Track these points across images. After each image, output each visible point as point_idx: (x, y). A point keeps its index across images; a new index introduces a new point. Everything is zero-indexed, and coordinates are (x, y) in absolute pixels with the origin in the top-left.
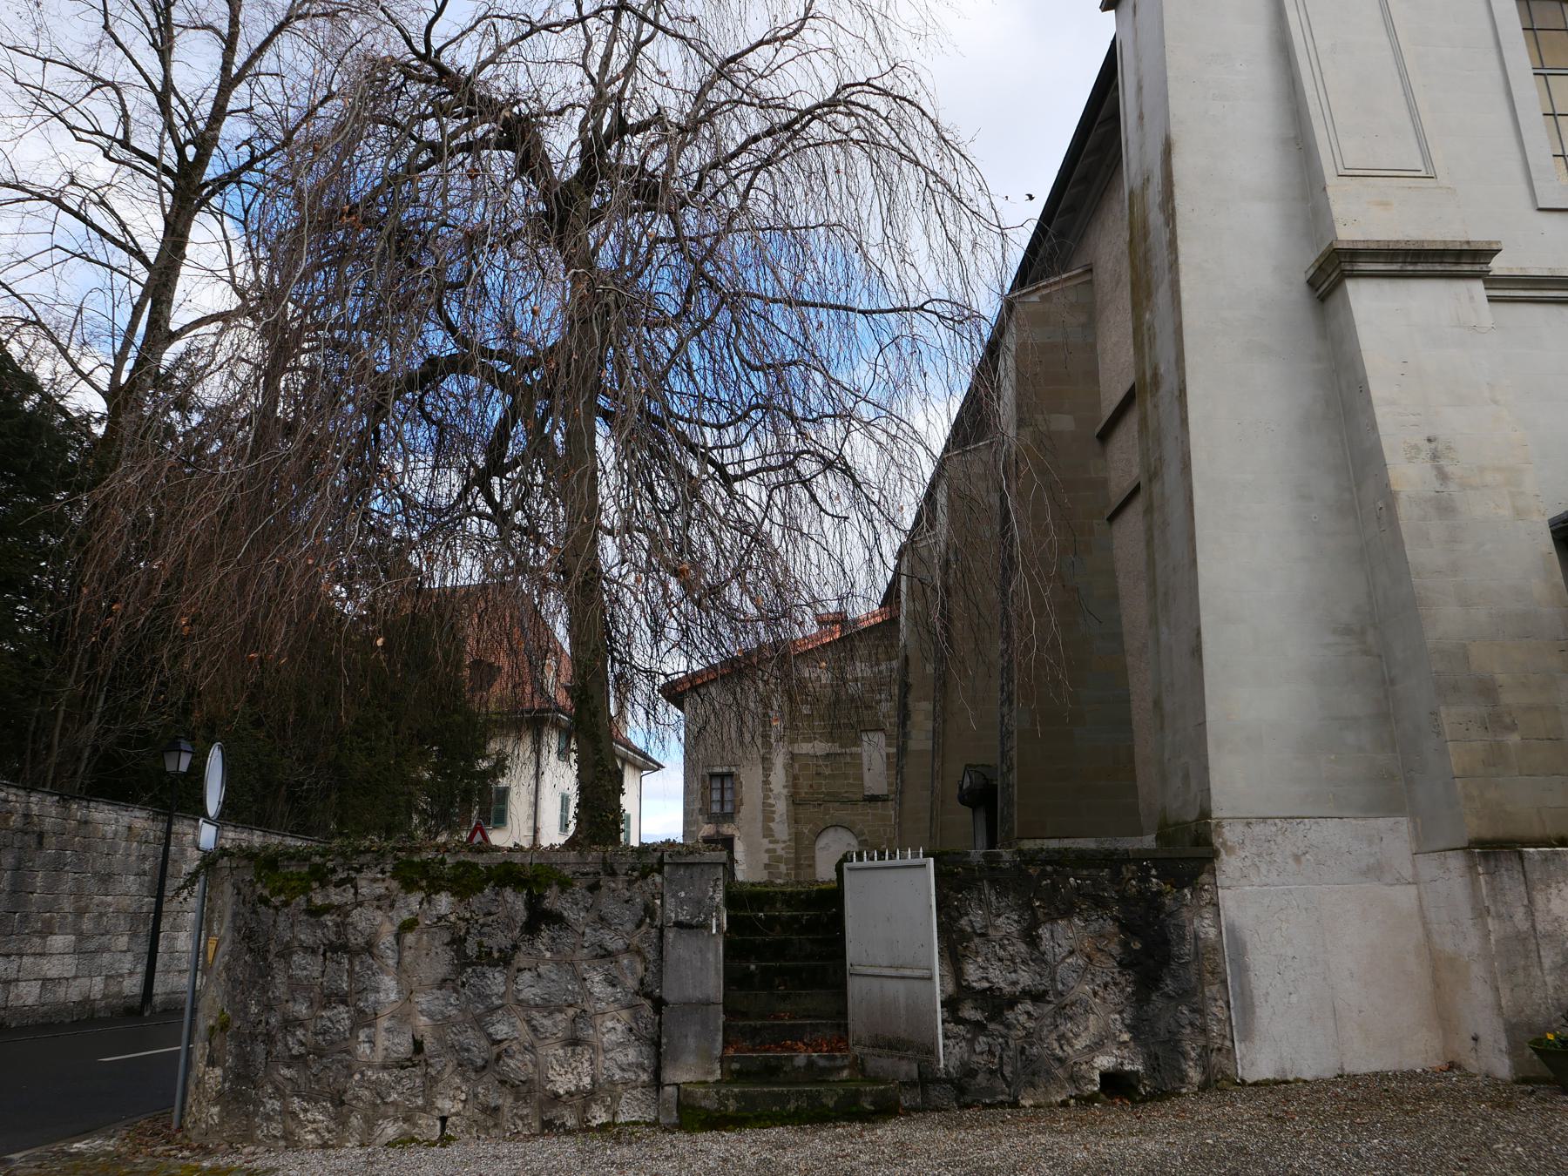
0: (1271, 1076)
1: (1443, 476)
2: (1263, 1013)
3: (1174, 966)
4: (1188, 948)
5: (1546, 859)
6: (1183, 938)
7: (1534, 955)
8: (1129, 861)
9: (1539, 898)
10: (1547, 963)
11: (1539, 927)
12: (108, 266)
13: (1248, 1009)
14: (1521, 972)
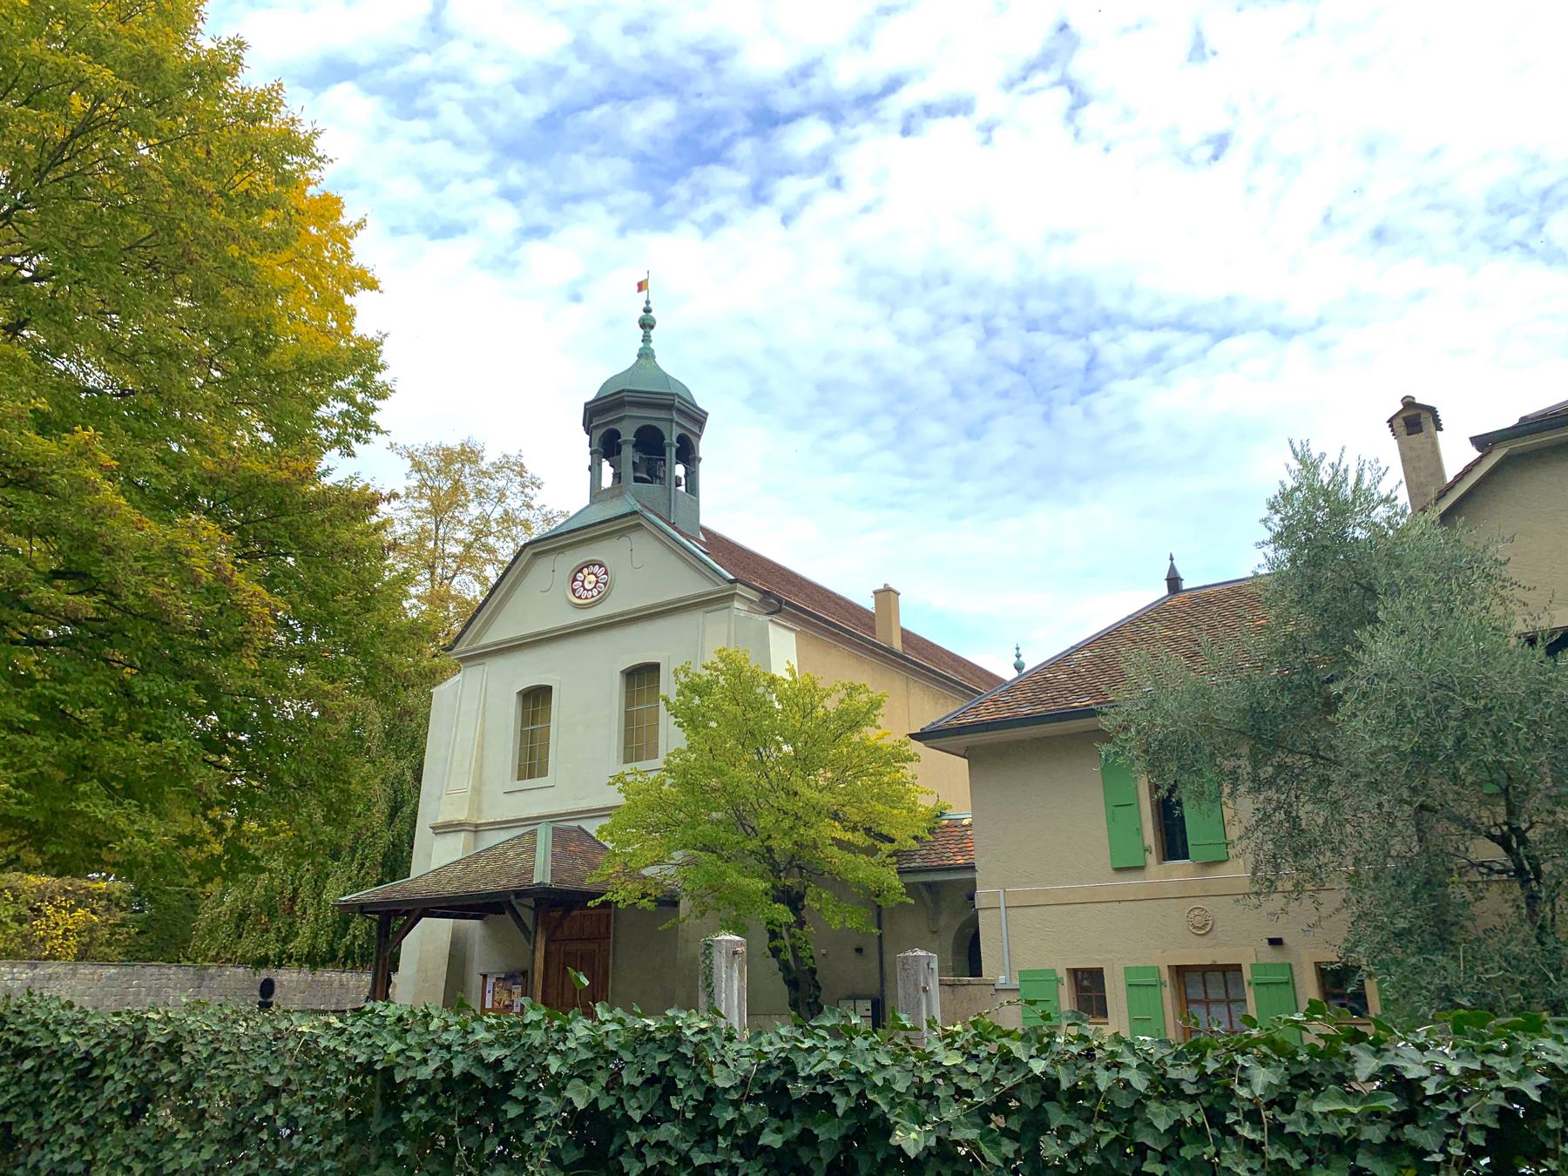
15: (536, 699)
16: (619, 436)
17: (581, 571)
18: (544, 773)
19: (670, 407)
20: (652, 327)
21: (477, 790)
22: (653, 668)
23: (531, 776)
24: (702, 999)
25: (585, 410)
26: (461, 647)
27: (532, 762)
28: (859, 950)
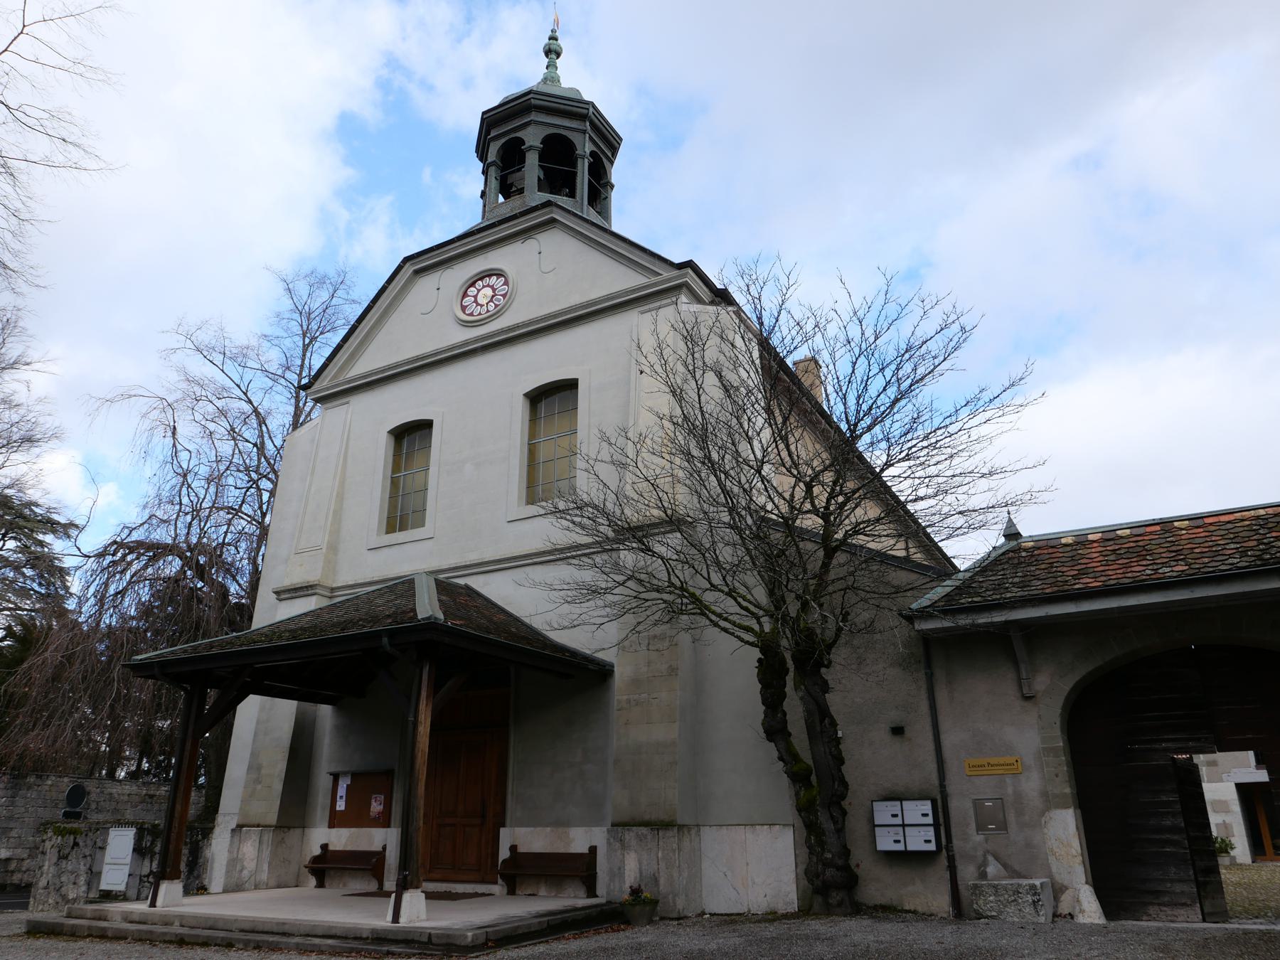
15: (411, 436)
16: (524, 143)
17: (473, 285)
18: (421, 523)
19: (583, 117)
20: (558, 55)
21: (333, 548)
22: (568, 387)
23: (403, 528)
24: (534, 510)
25: (483, 120)
26: (323, 384)
27: (402, 512)
28: (898, 731)
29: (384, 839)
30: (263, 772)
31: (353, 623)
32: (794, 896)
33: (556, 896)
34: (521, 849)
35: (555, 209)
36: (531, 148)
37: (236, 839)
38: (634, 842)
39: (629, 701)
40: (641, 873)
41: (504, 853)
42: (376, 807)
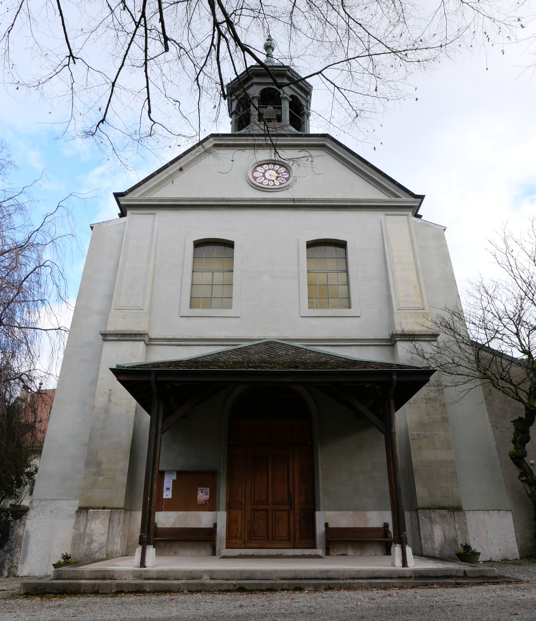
0: (26, 575)
1: (110, 401)
2: (29, 556)
3: (9, 542)
4: (13, 537)
5: (94, 513)
6: (13, 534)
7: (82, 540)
8: (4, 511)
9: (89, 524)
10: (86, 542)
11: (86, 532)
12: (146, 64)
13: (25, 555)
14: (77, 545)
29: (216, 519)
30: (104, 467)
31: (124, 367)
32: (516, 550)
33: (361, 555)
34: (331, 526)
35: (328, 140)
36: (253, 98)
37: (83, 519)
38: (438, 519)
39: (418, 435)
40: (445, 537)
41: (320, 529)
42: (202, 496)
